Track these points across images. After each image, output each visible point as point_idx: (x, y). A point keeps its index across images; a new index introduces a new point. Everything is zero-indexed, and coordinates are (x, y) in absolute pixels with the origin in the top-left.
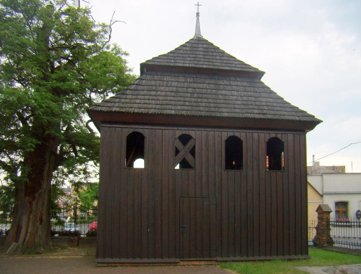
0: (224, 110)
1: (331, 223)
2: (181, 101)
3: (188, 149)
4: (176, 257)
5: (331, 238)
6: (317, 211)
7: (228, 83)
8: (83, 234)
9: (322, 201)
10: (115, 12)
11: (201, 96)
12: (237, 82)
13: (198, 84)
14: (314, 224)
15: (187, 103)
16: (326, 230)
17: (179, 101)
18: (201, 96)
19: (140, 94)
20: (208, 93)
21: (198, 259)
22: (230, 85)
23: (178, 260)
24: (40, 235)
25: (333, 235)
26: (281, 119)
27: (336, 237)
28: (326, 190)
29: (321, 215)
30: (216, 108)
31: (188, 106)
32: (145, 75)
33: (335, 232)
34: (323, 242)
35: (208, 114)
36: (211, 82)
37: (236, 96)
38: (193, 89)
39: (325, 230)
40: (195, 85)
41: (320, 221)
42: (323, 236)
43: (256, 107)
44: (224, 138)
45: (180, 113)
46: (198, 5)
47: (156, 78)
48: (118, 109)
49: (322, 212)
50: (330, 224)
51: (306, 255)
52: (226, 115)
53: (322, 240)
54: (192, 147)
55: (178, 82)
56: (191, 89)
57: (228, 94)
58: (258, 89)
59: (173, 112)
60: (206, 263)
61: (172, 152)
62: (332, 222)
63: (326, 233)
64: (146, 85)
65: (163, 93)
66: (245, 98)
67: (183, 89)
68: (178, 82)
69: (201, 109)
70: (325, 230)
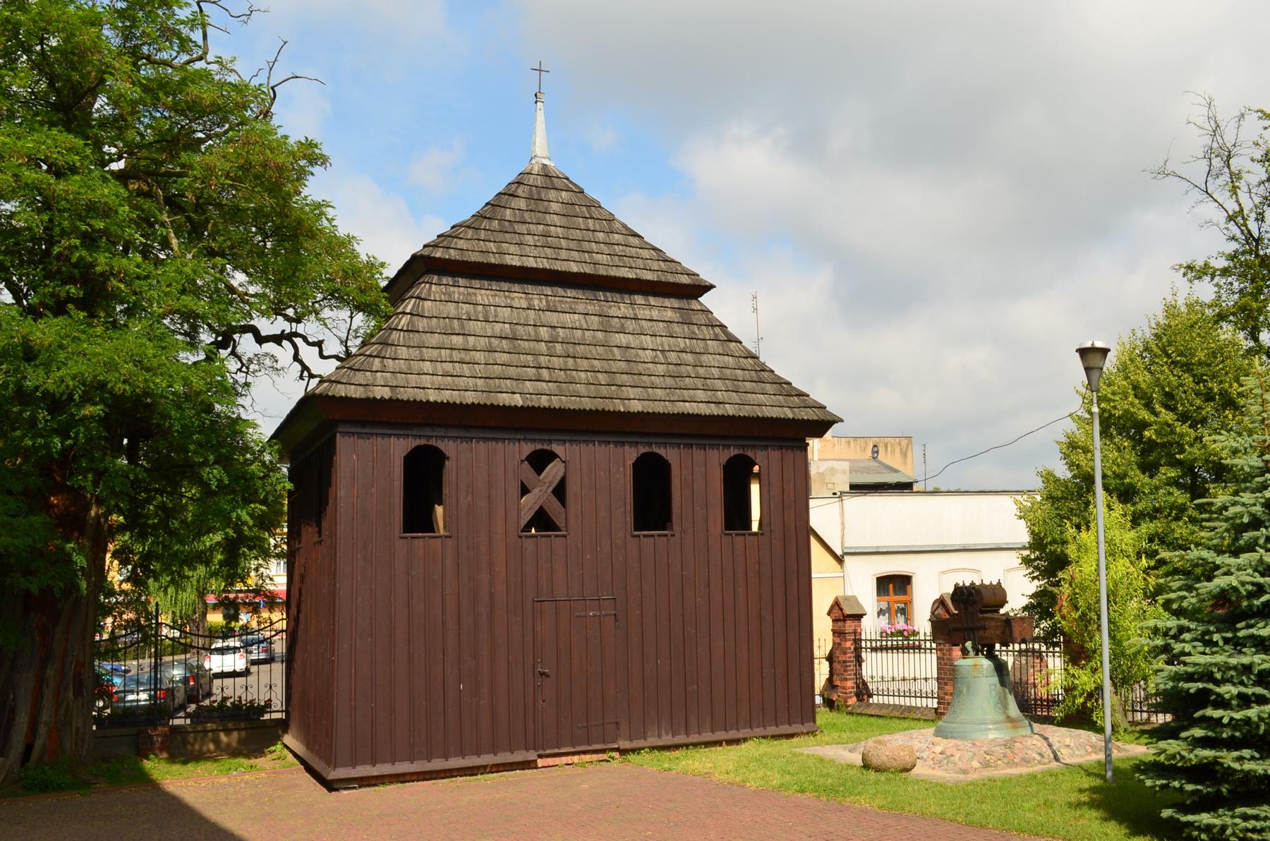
0: (632, 392)
1: (863, 644)
2: (529, 367)
3: (549, 487)
4: (527, 750)
5: (865, 684)
6: (829, 613)
7: (630, 313)
8: (278, 711)
9: (842, 575)
10: (285, 43)
11: (571, 349)
12: (650, 309)
13: (561, 314)
14: (823, 648)
15: (545, 374)
16: (852, 662)
17: (524, 367)
18: (571, 349)
19: (427, 345)
20: (588, 342)
21: (578, 749)
22: (636, 319)
23: (532, 755)
24: (78, 729)
25: (869, 674)
26: (755, 416)
27: (875, 680)
28: (853, 542)
29: (840, 624)
30: (613, 387)
31: (548, 382)
32: (427, 285)
33: (875, 667)
34: (846, 693)
35: (598, 404)
36: (590, 308)
37: (652, 350)
38: (550, 329)
39: (849, 662)
40: (553, 318)
41: (838, 641)
42: (846, 679)
43: (699, 383)
44: (630, 462)
45: (534, 402)
46: (540, 70)
47: (457, 293)
48: (385, 393)
49: (845, 616)
50: (861, 648)
51: (812, 724)
52: (636, 406)
53: (844, 688)
54: (559, 478)
55: (511, 307)
56: (545, 328)
57: (633, 346)
58: (698, 329)
59: (518, 400)
60: (595, 757)
61: (514, 489)
62: (866, 640)
63: (853, 670)
64: (436, 317)
65: (483, 342)
66: (673, 357)
67: (526, 327)
68: (511, 307)
69: (581, 389)
70: (849, 662)
